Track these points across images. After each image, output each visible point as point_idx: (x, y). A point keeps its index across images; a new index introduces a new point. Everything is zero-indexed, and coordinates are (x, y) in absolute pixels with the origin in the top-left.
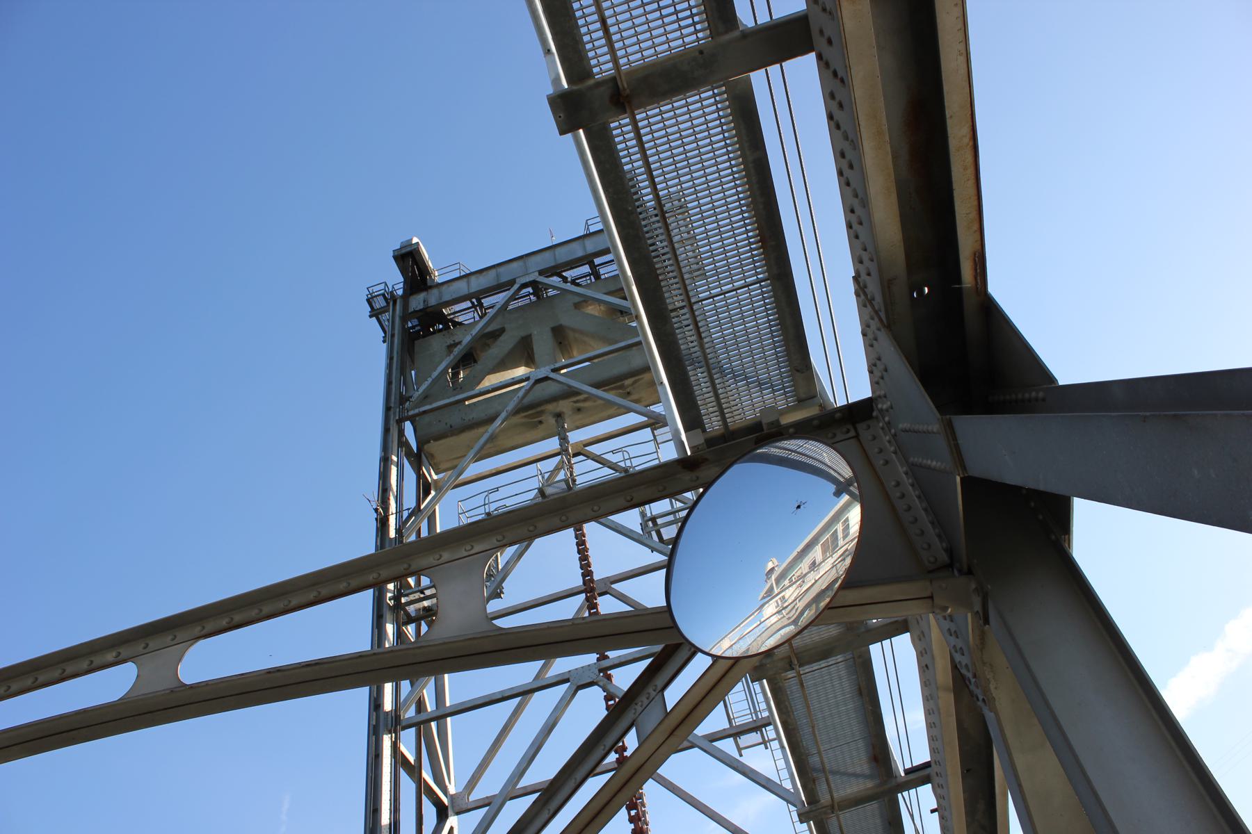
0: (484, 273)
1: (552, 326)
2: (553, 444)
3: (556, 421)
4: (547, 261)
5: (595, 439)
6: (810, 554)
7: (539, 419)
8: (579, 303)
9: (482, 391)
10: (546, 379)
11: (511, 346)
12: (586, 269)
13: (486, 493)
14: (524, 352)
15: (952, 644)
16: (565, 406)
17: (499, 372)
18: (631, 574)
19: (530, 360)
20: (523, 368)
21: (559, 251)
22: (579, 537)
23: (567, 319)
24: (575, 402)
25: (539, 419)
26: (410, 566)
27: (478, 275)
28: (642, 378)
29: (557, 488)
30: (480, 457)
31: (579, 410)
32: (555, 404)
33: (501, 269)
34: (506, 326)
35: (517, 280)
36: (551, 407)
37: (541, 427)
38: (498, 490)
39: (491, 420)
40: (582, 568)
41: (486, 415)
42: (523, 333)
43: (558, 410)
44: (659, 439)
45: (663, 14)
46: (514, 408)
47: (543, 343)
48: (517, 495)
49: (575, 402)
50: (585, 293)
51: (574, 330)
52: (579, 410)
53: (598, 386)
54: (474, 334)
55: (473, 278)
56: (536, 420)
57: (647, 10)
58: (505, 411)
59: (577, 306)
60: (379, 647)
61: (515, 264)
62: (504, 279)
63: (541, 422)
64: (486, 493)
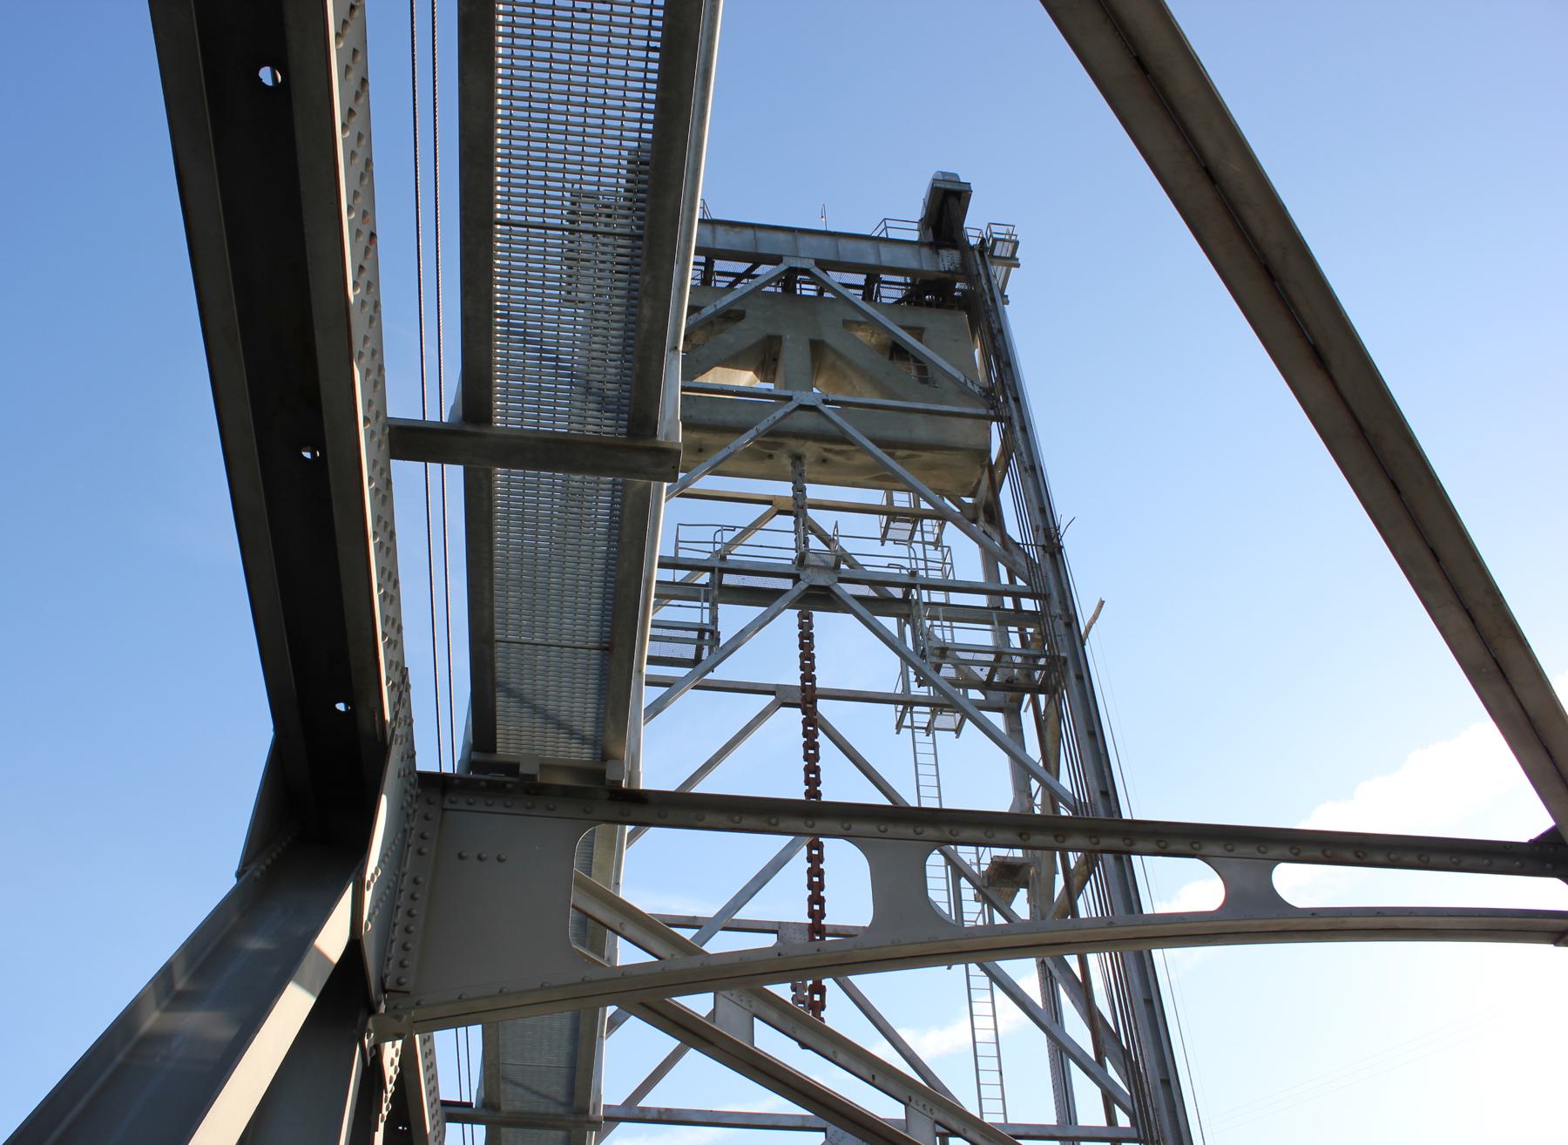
0: (737, 230)
1: (812, 337)
2: (784, 489)
3: (793, 464)
4: (826, 250)
5: (816, 503)
6: (596, 602)
7: (772, 452)
8: (850, 322)
9: (725, 389)
10: (813, 408)
11: (754, 340)
12: (860, 279)
13: (720, 528)
14: (766, 359)
15: (395, 590)
16: (810, 450)
17: (728, 367)
18: (837, 694)
19: (766, 371)
20: (751, 374)
21: (843, 243)
22: (805, 627)
23: (833, 337)
24: (825, 450)
25: (772, 452)
26: (1460, 862)
27: (727, 228)
28: (918, 456)
29: (823, 561)
30: (715, 471)
31: (824, 461)
32: (801, 442)
33: (761, 234)
34: (747, 311)
35: (785, 259)
36: (793, 444)
37: (768, 462)
38: (734, 530)
39: (740, 430)
40: (802, 668)
41: (710, 419)
42: (771, 331)
43: (801, 451)
44: (891, 534)
45: (647, 77)
46: (765, 430)
47: (794, 354)
48: (761, 546)
49: (825, 450)
50: (876, 317)
51: (839, 355)
52: (824, 461)
53: (879, 443)
54: (718, 307)
55: (720, 230)
56: (767, 451)
57: (649, 67)
58: (755, 428)
59: (847, 324)
60: (1141, 953)
61: (782, 236)
62: (764, 249)
63: (770, 456)
64: (720, 528)
